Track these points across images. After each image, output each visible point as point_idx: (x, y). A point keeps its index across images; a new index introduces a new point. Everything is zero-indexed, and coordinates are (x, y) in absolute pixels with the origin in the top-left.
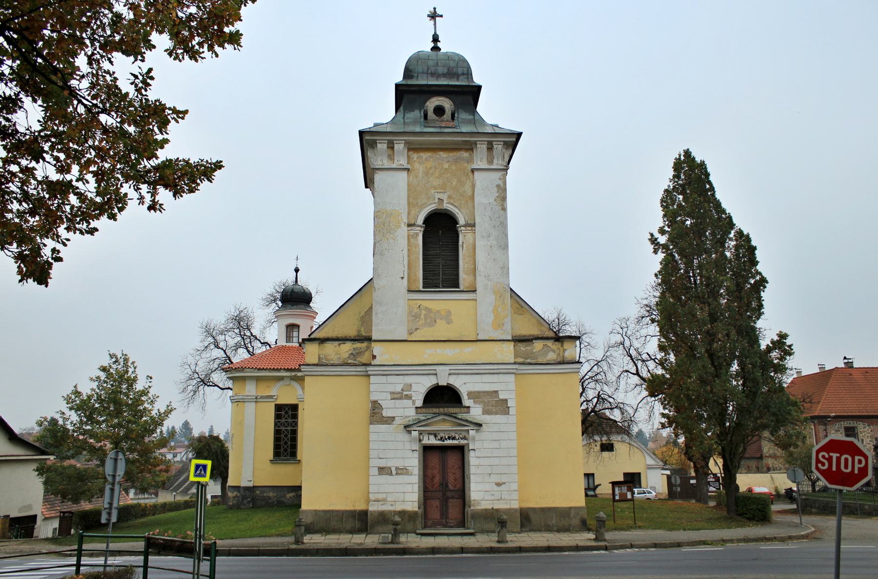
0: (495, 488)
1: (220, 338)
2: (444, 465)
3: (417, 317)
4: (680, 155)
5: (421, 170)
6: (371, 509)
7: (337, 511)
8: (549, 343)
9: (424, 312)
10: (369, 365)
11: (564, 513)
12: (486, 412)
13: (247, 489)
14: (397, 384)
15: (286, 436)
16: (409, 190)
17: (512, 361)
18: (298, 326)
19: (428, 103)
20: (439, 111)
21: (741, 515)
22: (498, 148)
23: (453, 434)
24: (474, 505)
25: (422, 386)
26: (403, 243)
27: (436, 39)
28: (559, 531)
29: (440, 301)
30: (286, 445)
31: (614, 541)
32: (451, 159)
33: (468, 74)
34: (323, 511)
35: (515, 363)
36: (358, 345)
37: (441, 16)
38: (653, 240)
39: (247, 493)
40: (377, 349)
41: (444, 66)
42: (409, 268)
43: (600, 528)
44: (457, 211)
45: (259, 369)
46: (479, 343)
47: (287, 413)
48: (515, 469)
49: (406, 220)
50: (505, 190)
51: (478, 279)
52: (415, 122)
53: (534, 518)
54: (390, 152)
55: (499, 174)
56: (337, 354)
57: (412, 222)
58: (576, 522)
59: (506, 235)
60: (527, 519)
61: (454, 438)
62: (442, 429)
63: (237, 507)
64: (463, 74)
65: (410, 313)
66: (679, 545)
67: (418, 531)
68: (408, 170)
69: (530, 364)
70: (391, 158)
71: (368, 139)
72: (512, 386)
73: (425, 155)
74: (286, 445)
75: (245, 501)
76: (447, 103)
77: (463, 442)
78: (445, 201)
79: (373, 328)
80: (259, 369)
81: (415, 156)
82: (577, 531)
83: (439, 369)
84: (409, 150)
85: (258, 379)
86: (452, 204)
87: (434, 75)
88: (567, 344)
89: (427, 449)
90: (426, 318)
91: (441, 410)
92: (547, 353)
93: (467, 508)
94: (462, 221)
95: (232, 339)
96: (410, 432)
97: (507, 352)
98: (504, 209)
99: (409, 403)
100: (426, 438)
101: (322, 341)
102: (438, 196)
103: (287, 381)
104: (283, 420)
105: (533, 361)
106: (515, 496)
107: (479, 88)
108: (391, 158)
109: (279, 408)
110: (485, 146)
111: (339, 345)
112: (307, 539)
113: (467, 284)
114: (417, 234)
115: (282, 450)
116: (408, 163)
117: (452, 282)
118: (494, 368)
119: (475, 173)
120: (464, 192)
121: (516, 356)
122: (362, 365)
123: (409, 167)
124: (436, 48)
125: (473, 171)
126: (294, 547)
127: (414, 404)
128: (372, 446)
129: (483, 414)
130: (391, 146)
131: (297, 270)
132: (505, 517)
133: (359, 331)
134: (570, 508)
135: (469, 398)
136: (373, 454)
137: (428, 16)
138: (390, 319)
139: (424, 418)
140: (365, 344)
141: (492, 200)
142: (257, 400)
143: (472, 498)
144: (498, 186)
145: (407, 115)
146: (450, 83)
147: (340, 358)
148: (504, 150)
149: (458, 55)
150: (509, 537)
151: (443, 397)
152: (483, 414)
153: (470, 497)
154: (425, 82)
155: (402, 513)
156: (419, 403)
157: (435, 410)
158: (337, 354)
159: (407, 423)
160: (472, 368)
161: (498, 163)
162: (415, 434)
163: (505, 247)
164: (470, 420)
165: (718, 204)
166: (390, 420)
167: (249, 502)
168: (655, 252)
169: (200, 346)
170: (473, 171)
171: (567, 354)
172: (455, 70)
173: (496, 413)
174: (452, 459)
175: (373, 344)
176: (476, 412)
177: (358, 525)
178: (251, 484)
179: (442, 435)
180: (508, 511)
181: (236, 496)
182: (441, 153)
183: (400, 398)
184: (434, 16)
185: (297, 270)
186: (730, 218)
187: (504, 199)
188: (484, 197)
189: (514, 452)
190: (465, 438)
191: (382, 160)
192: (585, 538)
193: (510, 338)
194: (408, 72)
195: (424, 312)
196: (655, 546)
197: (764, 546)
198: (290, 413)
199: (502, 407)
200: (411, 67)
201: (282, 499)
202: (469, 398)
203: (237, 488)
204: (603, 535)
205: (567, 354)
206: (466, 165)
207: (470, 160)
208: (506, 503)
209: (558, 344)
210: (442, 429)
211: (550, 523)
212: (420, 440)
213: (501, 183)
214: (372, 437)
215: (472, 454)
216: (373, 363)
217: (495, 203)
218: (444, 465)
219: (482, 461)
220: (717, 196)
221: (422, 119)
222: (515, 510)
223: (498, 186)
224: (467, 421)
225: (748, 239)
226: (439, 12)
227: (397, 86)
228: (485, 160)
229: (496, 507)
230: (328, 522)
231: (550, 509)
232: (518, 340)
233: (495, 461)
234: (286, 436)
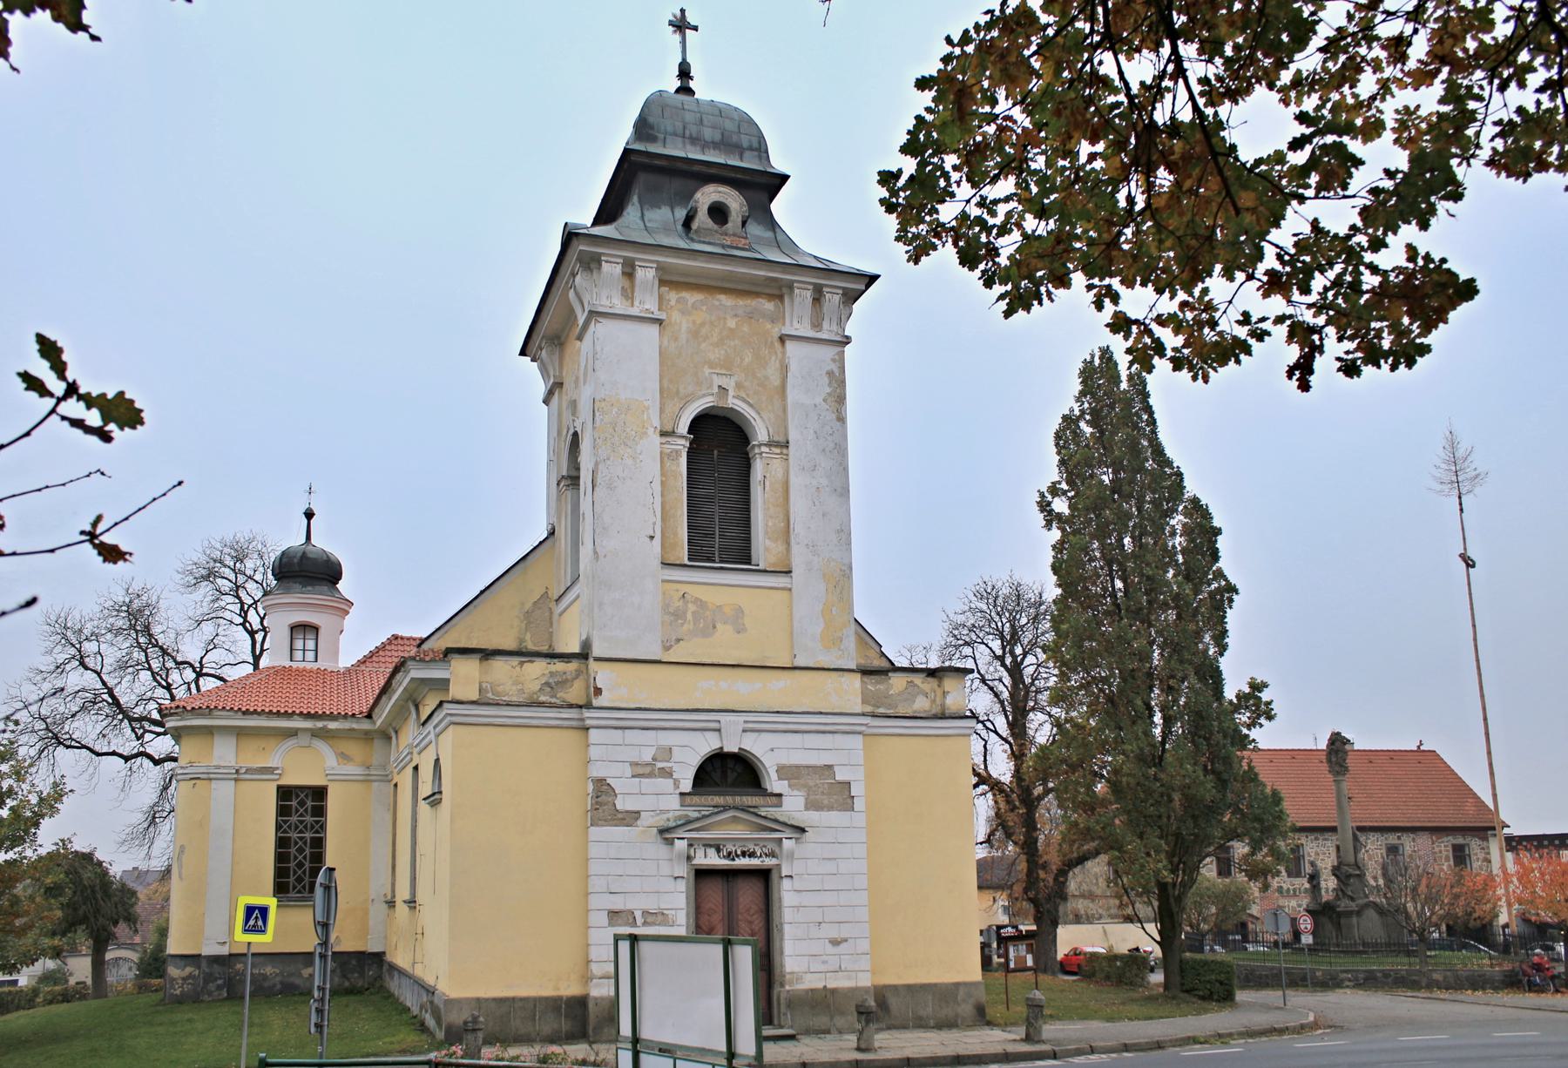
0: (830, 949)
1: (91, 647)
3: (678, 615)
4: (1093, 356)
5: (684, 326)
7: (522, 999)
8: (918, 679)
9: (692, 607)
10: (589, 706)
11: (947, 993)
12: (811, 805)
14: (644, 746)
15: (300, 850)
16: (662, 364)
18: (316, 629)
19: (698, 195)
20: (719, 213)
21: (1187, 991)
22: (833, 299)
23: (751, 847)
24: (791, 983)
25: (692, 751)
26: (652, 468)
27: (684, 73)
28: (940, 1026)
29: (718, 587)
31: (1058, 1042)
32: (740, 312)
33: (761, 149)
34: (495, 1000)
37: (695, 28)
38: (1044, 506)
39: (216, 968)
40: (603, 675)
41: (714, 127)
42: (663, 519)
43: (1036, 1018)
44: (754, 414)
45: (246, 713)
46: (797, 672)
47: (302, 803)
48: (863, 914)
49: (656, 423)
50: (842, 383)
51: (795, 549)
52: (666, 230)
53: (894, 1002)
54: (627, 284)
56: (516, 683)
57: (669, 428)
58: (967, 1009)
59: (846, 469)
61: (752, 855)
62: (730, 835)
63: (193, 998)
64: (751, 149)
65: (665, 608)
66: (1159, 1046)
68: (660, 322)
70: (628, 295)
72: (859, 757)
73: (692, 297)
75: (212, 986)
78: (731, 393)
80: (246, 713)
81: (673, 296)
82: (971, 1027)
83: (725, 718)
84: (662, 282)
85: (240, 733)
86: (744, 401)
87: (695, 140)
88: (949, 683)
89: (702, 874)
90: (696, 620)
91: (729, 800)
92: (915, 696)
93: (776, 989)
94: (761, 432)
95: (112, 652)
96: (670, 842)
97: (849, 694)
98: (842, 419)
99: (665, 784)
100: (700, 853)
102: (718, 381)
103: (304, 739)
104: (294, 819)
105: (890, 712)
106: (865, 963)
108: (628, 295)
109: (285, 793)
111: (522, 663)
113: (772, 559)
114: (678, 453)
115: (292, 879)
117: (740, 554)
118: (825, 722)
119: (789, 345)
120: (766, 378)
122: (579, 710)
123: (663, 316)
124: (685, 90)
125: (782, 339)
127: (676, 783)
128: (594, 868)
129: (807, 809)
130: (629, 272)
131: (309, 515)
133: (521, 641)
134: (957, 985)
135: (780, 779)
136: (596, 884)
139: (696, 815)
141: (819, 400)
142: (237, 776)
143: (788, 969)
144: (830, 374)
145: (649, 214)
147: (522, 691)
151: (729, 774)
152: (807, 809)
153: (782, 966)
156: (687, 786)
158: (516, 683)
159: (663, 823)
160: (784, 720)
162: (681, 845)
163: (844, 492)
165: (1158, 451)
166: (632, 817)
167: (219, 988)
168: (1048, 525)
169: (46, 663)
170: (782, 339)
171: (949, 701)
172: (735, 139)
173: (830, 808)
174: (748, 894)
176: (793, 806)
177: (565, 1026)
178: (225, 951)
179: (730, 848)
181: (190, 976)
182: (722, 297)
183: (650, 775)
185: (309, 515)
186: (1180, 475)
187: (841, 399)
188: (803, 394)
189: (862, 882)
190: (772, 855)
191: (609, 297)
194: (643, 127)
196: (1126, 1048)
197: (1301, 1044)
198: (309, 803)
199: (842, 797)
200: (651, 120)
201: (292, 979)
202: (780, 779)
203: (193, 959)
204: (870, 1039)
205: (949, 701)
206: (769, 326)
207: (777, 318)
208: (849, 978)
209: (933, 682)
210: (730, 835)
211: (922, 1013)
212: (689, 858)
213: (834, 367)
214: (594, 851)
215: (786, 884)
219: (808, 899)
220: (1160, 436)
221: (680, 227)
222: (866, 990)
223: (830, 374)
224: (776, 821)
225: (1206, 514)
228: (807, 322)
229: (831, 985)
233: (828, 898)
234: (300, 850)
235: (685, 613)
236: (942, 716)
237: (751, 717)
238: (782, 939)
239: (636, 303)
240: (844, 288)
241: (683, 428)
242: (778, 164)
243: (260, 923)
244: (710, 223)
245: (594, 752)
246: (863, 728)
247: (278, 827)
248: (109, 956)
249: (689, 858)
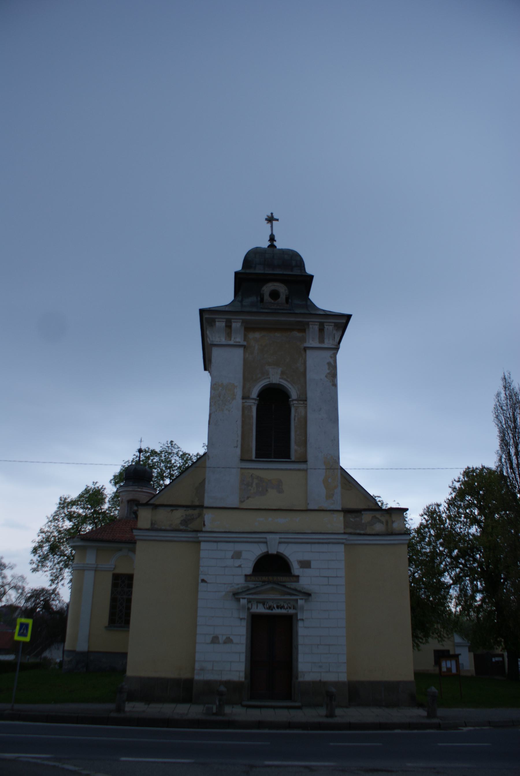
2: (272, 639)
6: (196, 678)
10: (201, 531)
13: (82, 653)
17: (342, 531)
20: (275, 295)
22: (329, 328)
23: (282, 604)
25: (253, 553)
27: (272, 239)
29: (270, 470)
30: (120, 613)
35: (345, 533)
36: (190, 512)
37: (277, 220)
55: (332, 352)
60: (356, 692)
61: (282, 607)
67: (245, 703)
68: (244, 347)
69: (360, 534)
70: (229, 335)
71: (208, 317)
74: (120, 613)
76: (282, 289)
77: (291, 611)
79: (206, 495)
83: (269, 536)
91: (271, 578)
94: (294, 394)
100: (254, 606)
101: (156, 507)
105: (362, 532)
107: (311, 277)
108: (229, 335)
110: (317, 328)
111: (172, 510)
112: (129, 707)
116: (245, 340)
119: (308, 352)
121: (346, 526)
123: (245, 343)
124: (272, 246)
125: (305, 349)
126: (113, 715)
130: (229, 326)
132: (333, 690)
137: (266, 219)
138: (222, 488)
140: (196, 512)
144: (329, 364)
146: (285, 273)
148: (335, 332)
149: (292, 251)
150: (338, 711)
153: (297, 667)
154: (262, 272)
155: (227, 683)
156: (249, 570)
157: (265, 578)
161: (328, 343)
162: (243, 602)
164: (299, 589)
170: (305, 349)
175: (205, 511)
179: (271, 603)
180: (336, 684)
184: (271, 219)
192: (418, 714)
193: (340, 508)
194: (248, 261)
207: (304, 340)
212: (249, 609)
215: (300, 624)
216: (204, 529)
218: (272, 639)
223: (329, 364)
224: (296, 590)
226: (275, 217)
227: (237, 274)
230: (153, 690)
232: (347, 512)
236: (392, 534)
237: (283, 536)
238: (297, 654)
239: (232, 339)
240: (335, 323)
241: (255, 393)
243: (25, 631)
244: (270, 300)
245: (203, 554)
246: (344, 541)
247: (112, 593)
249: (249, 609)
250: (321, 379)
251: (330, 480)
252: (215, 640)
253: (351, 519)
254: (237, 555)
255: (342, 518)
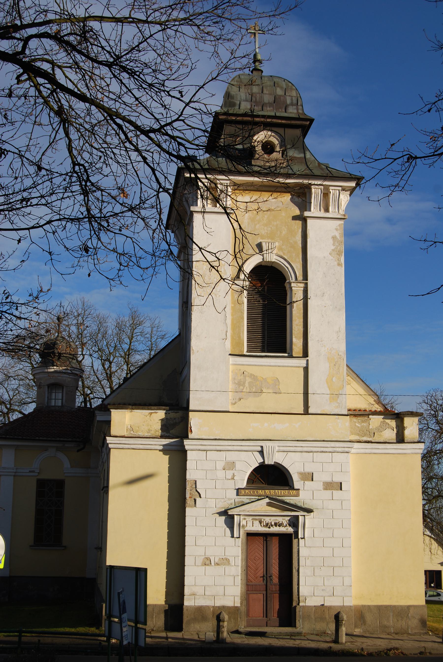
25: (250, 462)
134: (409, 607)
151: (271, 477)
164: (299, 504)
195: (248, 380)
217: (331, 257)
218: (275, 559)
231: (387, 607)
235: (244, 383)
237: (281, 443)
242: (309, 112)
248: (410, 632)
250: (324, 257)
251: (334, 379)
252: (207, 562)
253: (357, 424)
254: (231, 466)
255: (348, 424)
